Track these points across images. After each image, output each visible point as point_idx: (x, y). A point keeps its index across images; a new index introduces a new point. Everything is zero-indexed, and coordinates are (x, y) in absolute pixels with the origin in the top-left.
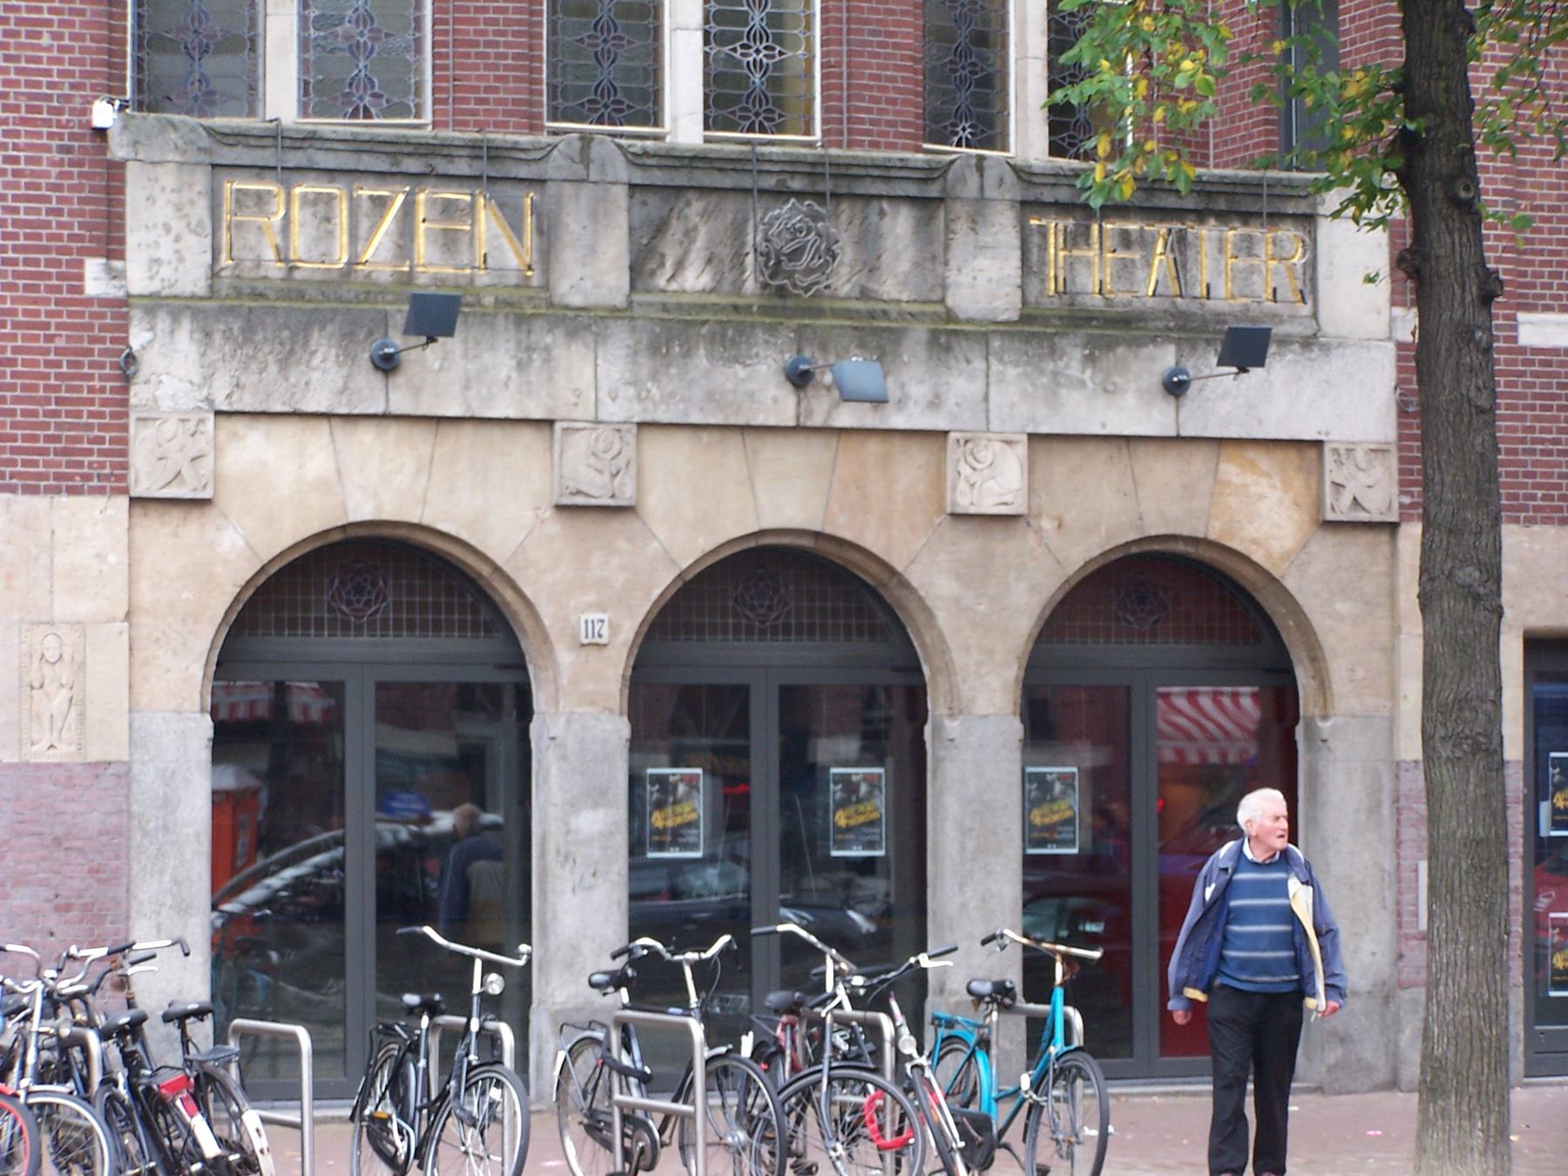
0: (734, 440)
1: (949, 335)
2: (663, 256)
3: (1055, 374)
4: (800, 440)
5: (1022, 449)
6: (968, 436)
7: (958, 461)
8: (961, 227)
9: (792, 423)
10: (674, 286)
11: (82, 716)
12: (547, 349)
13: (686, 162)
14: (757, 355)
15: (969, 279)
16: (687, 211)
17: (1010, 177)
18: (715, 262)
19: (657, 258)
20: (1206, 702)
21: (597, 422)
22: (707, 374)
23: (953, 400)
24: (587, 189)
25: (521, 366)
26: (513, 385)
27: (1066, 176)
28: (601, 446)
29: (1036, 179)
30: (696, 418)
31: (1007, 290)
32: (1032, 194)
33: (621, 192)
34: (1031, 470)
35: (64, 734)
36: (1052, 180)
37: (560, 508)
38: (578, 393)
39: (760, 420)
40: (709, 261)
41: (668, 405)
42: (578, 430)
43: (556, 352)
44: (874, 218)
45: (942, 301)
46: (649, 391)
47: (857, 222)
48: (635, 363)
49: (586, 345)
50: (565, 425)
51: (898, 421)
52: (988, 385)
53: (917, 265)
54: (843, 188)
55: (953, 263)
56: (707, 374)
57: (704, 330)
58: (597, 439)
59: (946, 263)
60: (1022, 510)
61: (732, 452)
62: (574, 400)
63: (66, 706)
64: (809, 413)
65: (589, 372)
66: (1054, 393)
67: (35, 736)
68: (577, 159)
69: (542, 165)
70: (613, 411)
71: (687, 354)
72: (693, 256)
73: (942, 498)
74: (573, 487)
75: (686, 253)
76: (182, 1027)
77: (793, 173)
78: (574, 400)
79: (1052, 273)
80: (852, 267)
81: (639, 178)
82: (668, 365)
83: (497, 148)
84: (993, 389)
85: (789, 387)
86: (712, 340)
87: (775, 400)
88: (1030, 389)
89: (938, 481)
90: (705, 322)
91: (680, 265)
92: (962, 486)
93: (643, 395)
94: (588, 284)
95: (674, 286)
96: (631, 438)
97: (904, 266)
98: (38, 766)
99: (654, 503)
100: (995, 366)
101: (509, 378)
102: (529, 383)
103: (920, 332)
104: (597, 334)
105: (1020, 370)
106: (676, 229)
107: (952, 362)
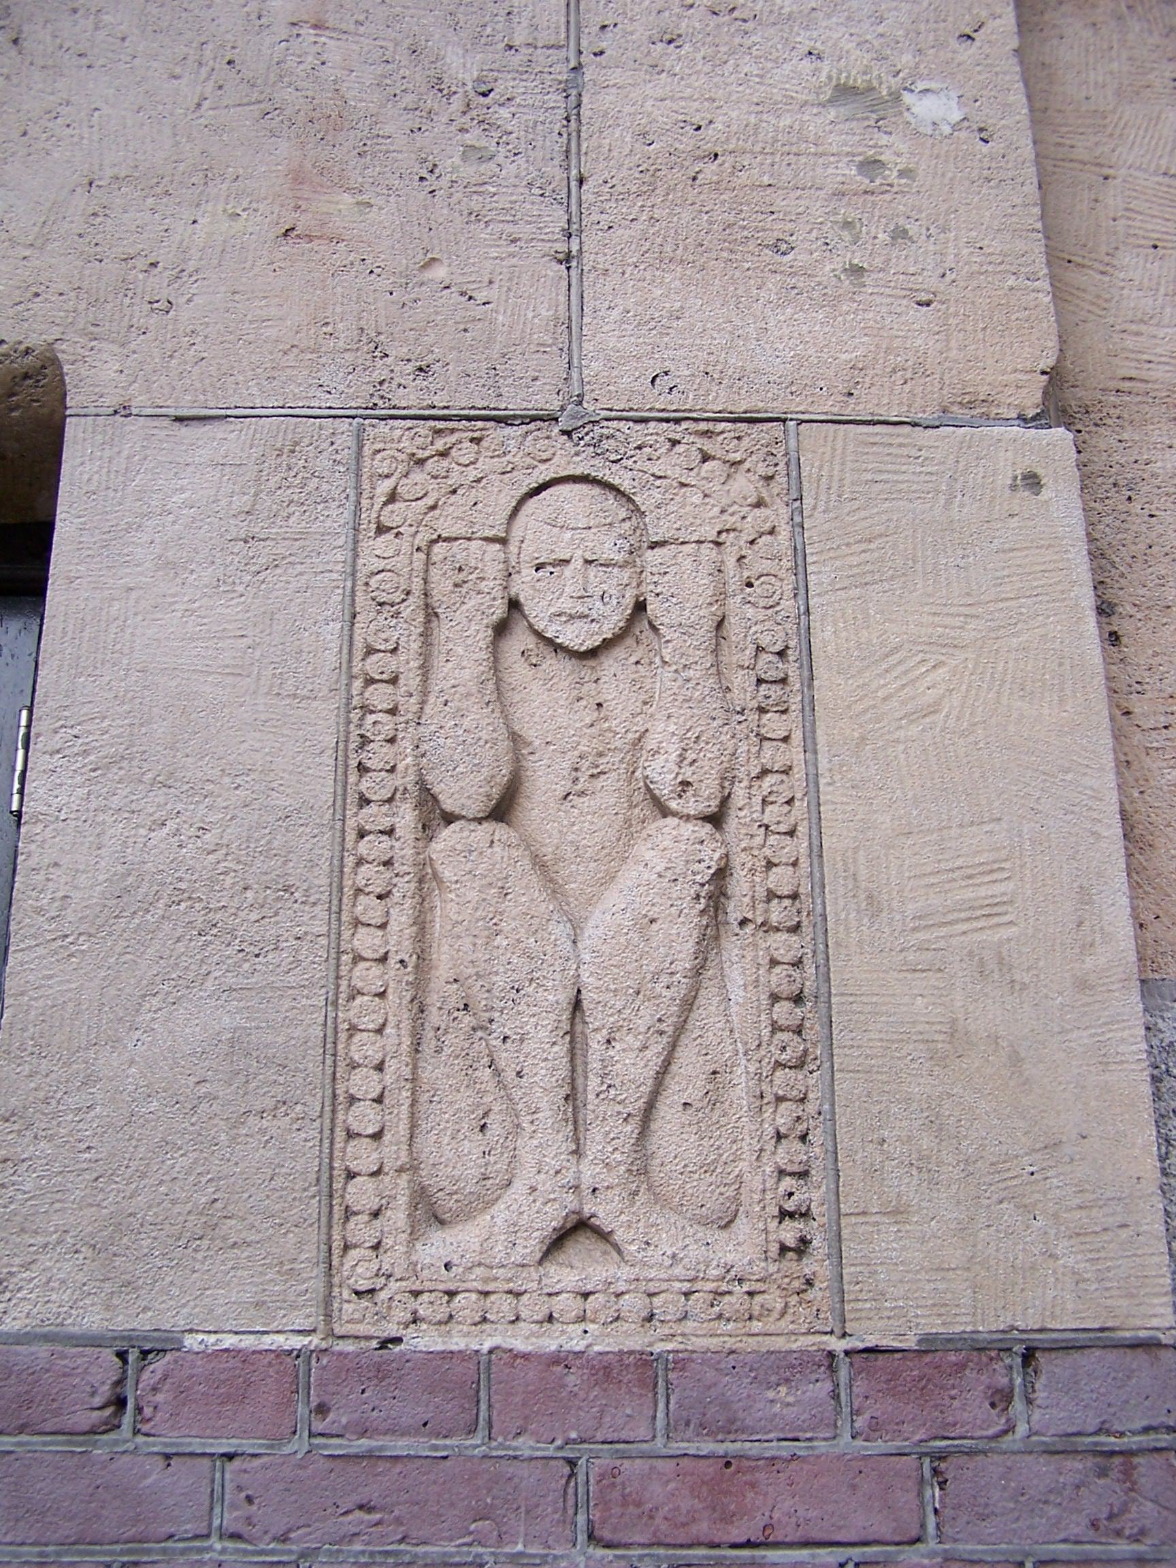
11: (801, 1002)
35: (672, 1134)
63: (679, 936)
67: (454, 1158)
98: (471, 1386)
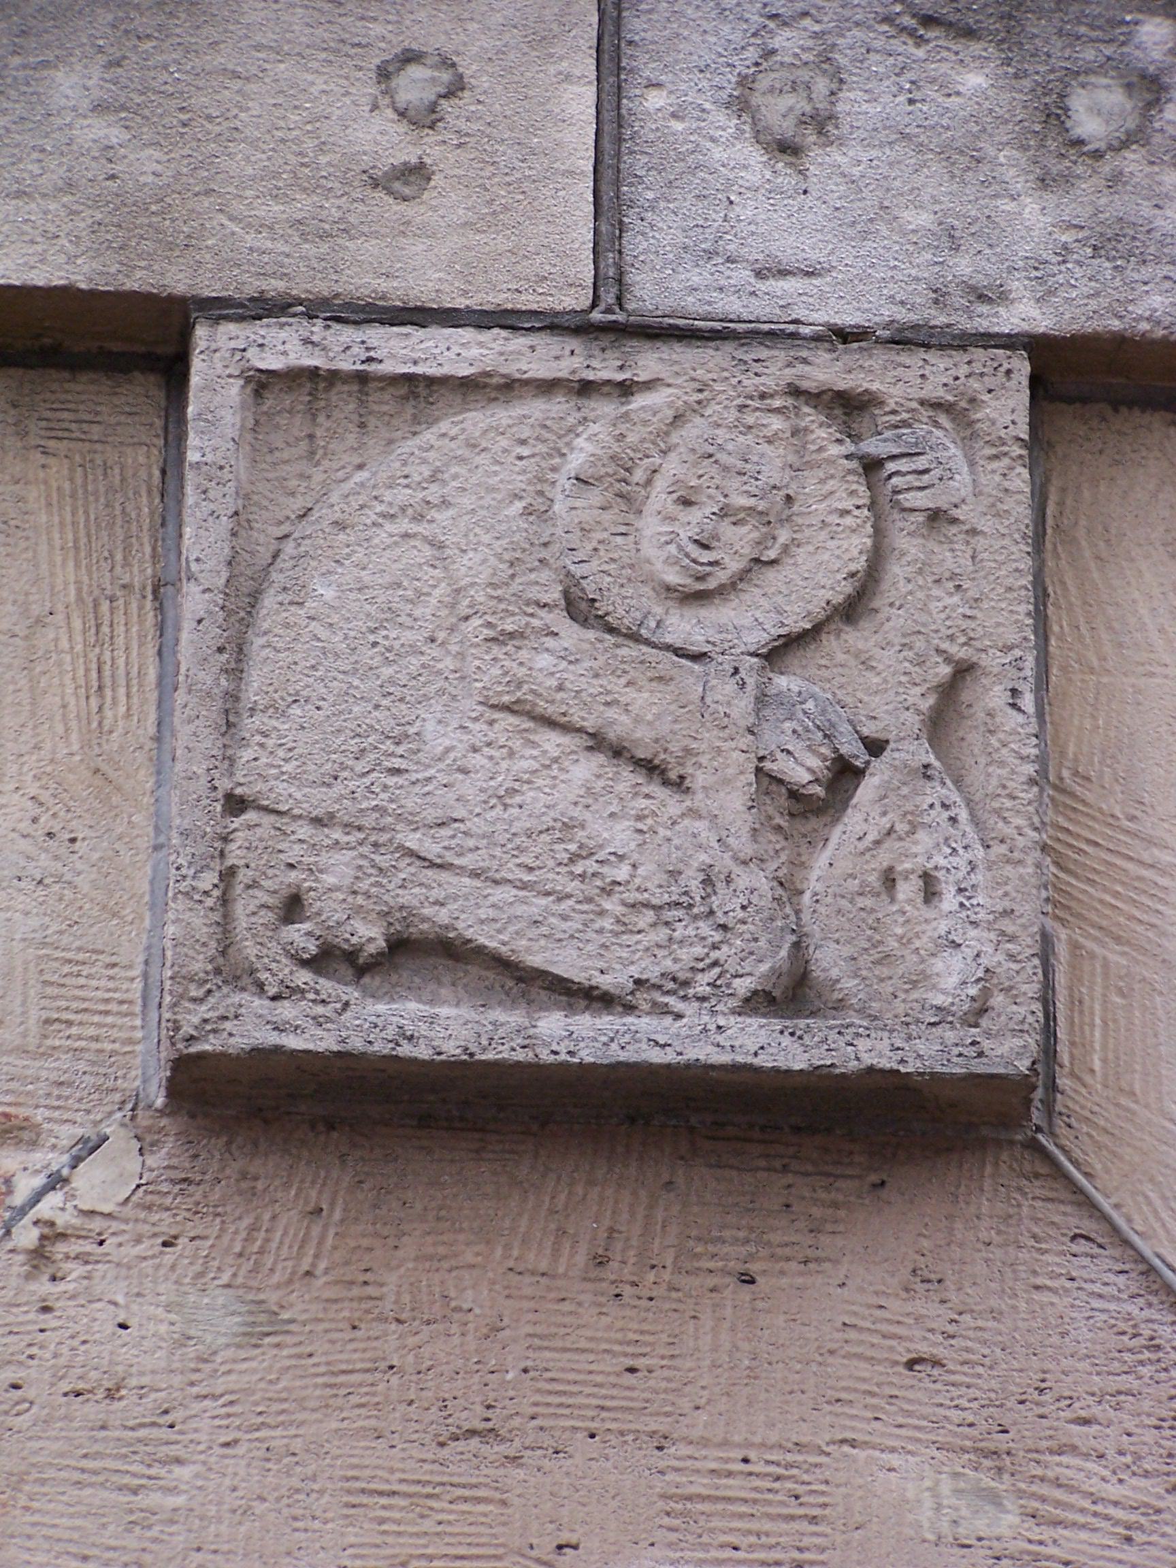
21: (613, 324)
28: (659, 539)
42: (420, 391)
50: (283, 346)
58: (621, 484)
62: (383, 140)
74: (349, 896)
76: (611, 276)
78: (383, 140)
90: (1105, 1001)
96: (982, 478)
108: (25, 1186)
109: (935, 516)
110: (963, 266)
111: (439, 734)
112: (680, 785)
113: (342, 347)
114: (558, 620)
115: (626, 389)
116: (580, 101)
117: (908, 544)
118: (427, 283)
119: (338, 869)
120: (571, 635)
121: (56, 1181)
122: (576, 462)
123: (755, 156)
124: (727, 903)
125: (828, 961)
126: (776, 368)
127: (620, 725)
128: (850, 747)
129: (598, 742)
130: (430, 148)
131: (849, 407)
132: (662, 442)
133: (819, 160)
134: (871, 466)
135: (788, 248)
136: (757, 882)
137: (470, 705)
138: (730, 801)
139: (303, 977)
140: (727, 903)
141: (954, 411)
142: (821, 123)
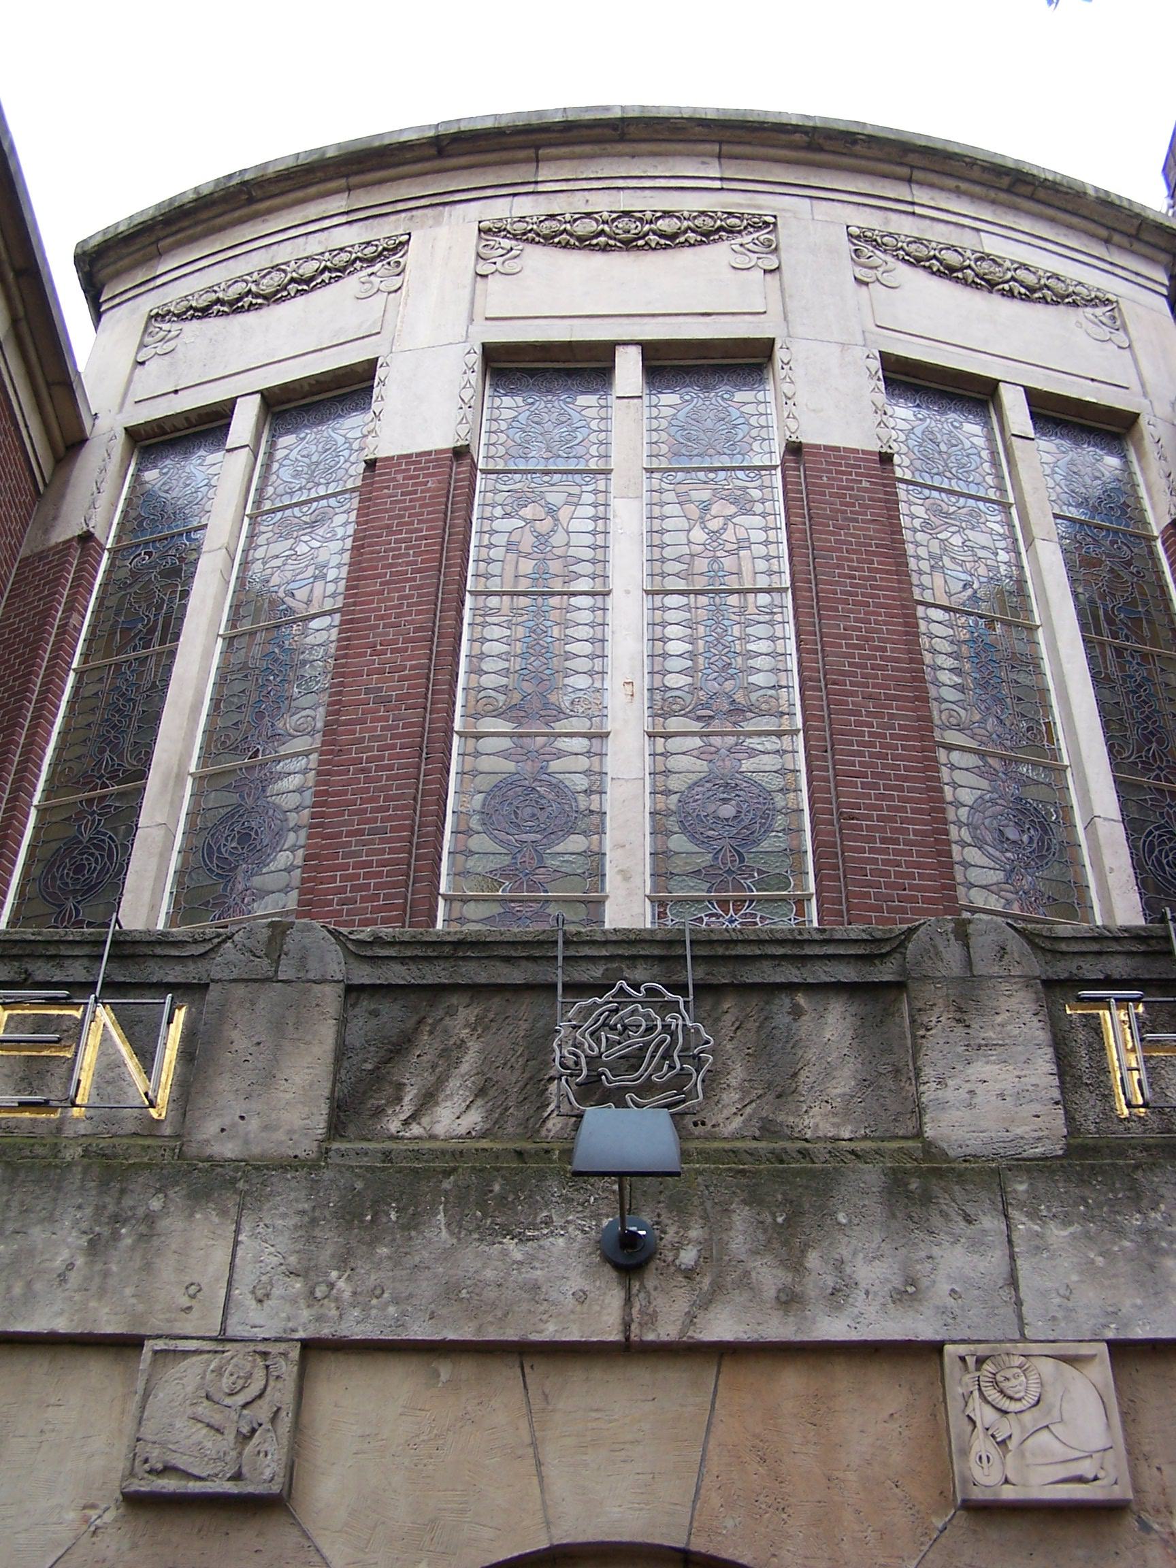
0: (506, 1374)
1: (924, 1181)
2: (400, 1086)
3: (1147, 1234)
4: (641, 1373)
5: (1101, 1370)
6: (982, 1349)
7: (966, 1398)
8: (939, 1019)
9: (615, 1336)
10: (416, 1130)
12: (150, 1219)
13: (447, 950)
14: (548, 1222)
15: (963, 1094)
16: (448, 1021)
17: (1016, 945)
18: (492, 1092)
19: (389, 1090)
20: (325, 621)
22: (447, 1254)
23: (944, 1287)
24: (269, 996)
25: (95, 1247)
26: (74, 1278)
27: (1116, 939)
28: (226, 1382)
29: (1063, 947)
30: (419, 1331)
31: (1037, 1108)
32: (1062, 969)
33: (330, 997)
34: (1129, 1417)
36: (1095, 947)
37: (135, 1502)
38: (194, 1290)
39: (550, 1332)
40: (481, 1092)
41: (366, 1308)
42: (186, 1353)
43: (164, 1224)
44: (782, 1019)
45: (919, 1135)
46: (331, 1286)
47: (752, 1025)
48: (311, 1239)
49: (223, 1213)
50: (160, 1345)
51: (833, 1328)
52: (1012, 1257)
53: (865, 1083)
54: (722, 976)
55: (928, 1072)
56: (447, 1254)
57: (447, 1185)
58: (219, 1372)
59: (918, 1072)
60: (1122, 1492)
61: (499, 1401)
62: (185, 1301)
64: (651, 1318)
65: (221, 1255)
66: (1152, 1267)
68: (261, 950)
69: (203, 966)
70: (255, 1320)
71: (412, 1223)
72: (453, 1083)
73: (947, 1473)
74: (157, 1458)
75: (441, 1082)
76: (223, 1330)
77: (633, 958)
79: (1118, 1076)
80: (745, 1092)
81: (364, 975)
82: (373, 1242)
83: (134, 943)
84: (1024, 1266)
85: (610, 1273)
86: (460, 1199)
87: (581, 1297)
88: (1100, 1261)
89: (938, 1445)
91: (428, 1099)
92: (981, 1445)
93: (320, 1291)
94: (254, 1124)
95: (416, 1130)
97: (842, 1085)
99: (329, 1492)
100: (1023, 1225)
101: (70, 1266)
102: (106, 1274)
103: (872, 1176)
104: (244, 1194)
105: (1076, 1228)
106: (427, 1046)
107: (937, 1221)
108: (94, 1517)
109: (278, 1377)
110: (290, 1325)
111: (179, 1424)
112: (222, 1433)
113: (171, 1345)
114: (204, 1400)
115: (223, 1352)
116: (223, 1292)
117: (272, 1383)
118: (189, 1331)
119: (156, 1453)
120: (206, 1403)
121: (100, 1517)
122: (212, 1367)
123: (254, 1302)
124: (228, 1458)
125: (245, 1470)
126: (251, 1347)
127: (212, 1422)
128: (255, 1426)
129: (208, 1425)
130: (193, 1303)
131: (265, 1355)
132: (228, 1362)
133: (267, 1303)
134: (267, 1367)
135: (257, 1322)
136: (234, 1454)
137: (185, 1418)
138: (230, 1436)
139: (146, 1475)
140: (228, 1458)
141: (284, 1355)
142: (267, 1295)
